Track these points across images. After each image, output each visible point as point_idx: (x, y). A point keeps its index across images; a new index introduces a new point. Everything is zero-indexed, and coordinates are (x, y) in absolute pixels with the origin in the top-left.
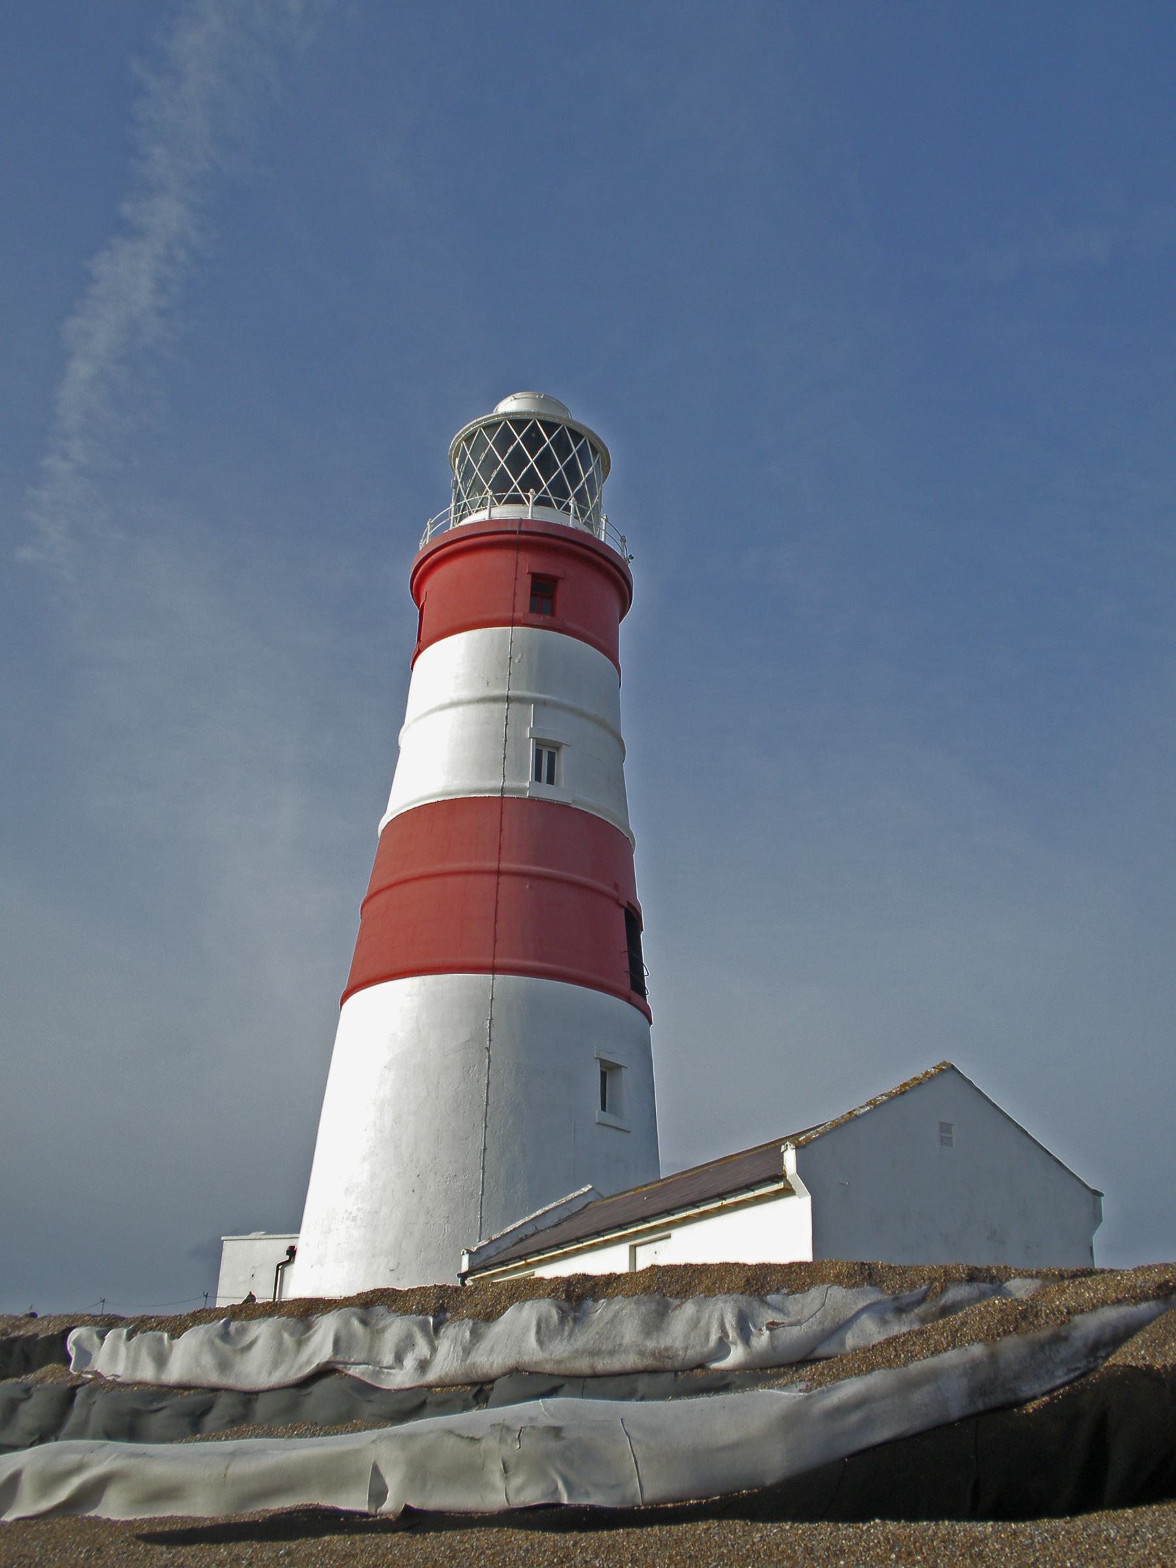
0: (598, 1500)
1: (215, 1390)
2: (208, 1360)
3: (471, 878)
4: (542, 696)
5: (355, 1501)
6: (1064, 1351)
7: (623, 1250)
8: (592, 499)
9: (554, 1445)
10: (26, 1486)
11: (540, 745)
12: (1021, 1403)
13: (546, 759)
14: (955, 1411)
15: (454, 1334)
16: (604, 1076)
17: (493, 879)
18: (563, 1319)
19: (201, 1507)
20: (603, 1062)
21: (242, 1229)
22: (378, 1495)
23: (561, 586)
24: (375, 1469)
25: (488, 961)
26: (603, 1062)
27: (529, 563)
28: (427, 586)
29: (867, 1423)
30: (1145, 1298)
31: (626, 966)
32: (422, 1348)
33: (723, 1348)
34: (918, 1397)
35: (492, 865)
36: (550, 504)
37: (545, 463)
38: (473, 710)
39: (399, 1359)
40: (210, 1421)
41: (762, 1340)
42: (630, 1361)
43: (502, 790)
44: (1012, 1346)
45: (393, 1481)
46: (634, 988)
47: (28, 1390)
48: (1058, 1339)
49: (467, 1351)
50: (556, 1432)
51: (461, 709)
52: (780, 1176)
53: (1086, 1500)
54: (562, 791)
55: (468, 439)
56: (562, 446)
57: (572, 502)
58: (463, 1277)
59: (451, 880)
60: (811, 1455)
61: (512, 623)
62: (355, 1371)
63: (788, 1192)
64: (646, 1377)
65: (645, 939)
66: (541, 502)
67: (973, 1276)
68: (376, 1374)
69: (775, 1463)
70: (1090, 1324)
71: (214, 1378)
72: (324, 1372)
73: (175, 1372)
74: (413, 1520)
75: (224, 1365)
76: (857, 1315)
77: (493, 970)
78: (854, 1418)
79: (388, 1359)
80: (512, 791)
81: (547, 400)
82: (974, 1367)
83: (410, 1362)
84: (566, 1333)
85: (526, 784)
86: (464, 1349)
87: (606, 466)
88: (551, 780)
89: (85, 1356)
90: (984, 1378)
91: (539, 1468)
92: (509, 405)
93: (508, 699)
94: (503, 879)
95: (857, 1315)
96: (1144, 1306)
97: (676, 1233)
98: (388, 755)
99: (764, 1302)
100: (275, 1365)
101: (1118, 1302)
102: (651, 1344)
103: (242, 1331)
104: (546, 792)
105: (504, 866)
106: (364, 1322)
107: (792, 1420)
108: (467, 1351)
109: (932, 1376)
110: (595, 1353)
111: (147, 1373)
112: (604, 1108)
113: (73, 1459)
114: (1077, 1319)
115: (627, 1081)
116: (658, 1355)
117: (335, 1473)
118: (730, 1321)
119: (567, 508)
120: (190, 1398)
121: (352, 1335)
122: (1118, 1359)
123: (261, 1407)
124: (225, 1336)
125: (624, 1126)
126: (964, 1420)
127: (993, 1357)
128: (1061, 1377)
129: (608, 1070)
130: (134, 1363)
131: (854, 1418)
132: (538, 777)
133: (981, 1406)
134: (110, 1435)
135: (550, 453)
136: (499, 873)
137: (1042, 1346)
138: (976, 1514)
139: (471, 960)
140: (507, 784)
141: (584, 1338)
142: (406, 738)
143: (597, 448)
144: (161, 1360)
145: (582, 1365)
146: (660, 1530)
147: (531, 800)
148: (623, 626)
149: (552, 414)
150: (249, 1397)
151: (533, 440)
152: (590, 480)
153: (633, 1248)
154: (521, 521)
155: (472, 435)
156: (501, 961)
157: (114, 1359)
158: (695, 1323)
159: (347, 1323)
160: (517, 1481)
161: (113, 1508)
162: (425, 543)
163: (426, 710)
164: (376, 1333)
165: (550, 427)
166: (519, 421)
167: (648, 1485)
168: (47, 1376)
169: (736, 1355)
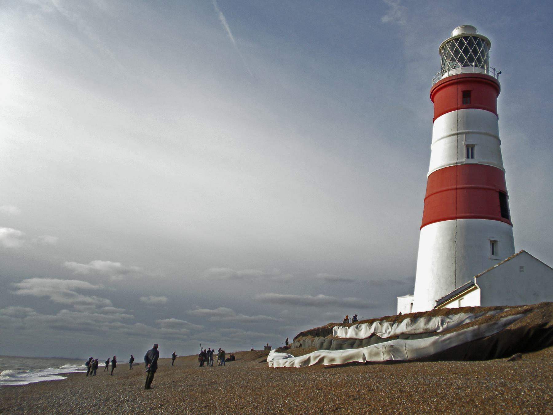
0: (399, 359)
1: (356, 339)
2: (354, 333)
3: (449, 191)
4: (467, 131)
5: (361, 360)
6: (496, 326)
7: (457, 301)
8: (483, 58)
9: (391, 349)
10: (312, 359)
11: (468, 147)
12: (485, 337)
14: (469, 340)
15: (395, 325)
17: (455, 190)
18: (411, 323)
19: (338, 362)
20: (491, 241)
21: (403, 294)
22: (364, 359)
23: (473, 93)
24: (364, 354)
25: (454, 215)
26: (491, 241)
27: (461, 88)
28: (438, 96)
29: (450, 343)
30: (520, 313)
31: (499, 209)
32: (390, 329)
33: (438, 328)
34: (461, 337)
35: (454, 187)
36: (468, 66)
37: (466, 51)
38: (447, 140)
39: (386, 331)
40: (355, 345)
41: (445, 326)
42: (421, 331)
43: (457, 163)
44: (484, 326)
45: (366, 356)
47: (325, 340)
48: (495, 324)
49: (395, 330)
50: (392, 346)
51: (444, 139)
52: (473, 285)
53: (490, 357)
55: (443, 47)
56: (470, 44)
58: (435, 307)
60: (439, 349)
61: (457, 109)
62: (378, 335)
63: (476, 288)
66: (464, 66)
67: (497, 308)
68: (382, 335)
69: (432, 351)
70: (504, 320)
71: (355, 337)
72: (373, 335)
73: (348, 336)
74: (368, 363)
75: (357, 334)
76: (466, 319)
77: (456, 218)
78: (447, 342)
79: (384, 332)
80: (460, 163)
81: (466, 27)
82: (474, 330)
83: (388, 332)
85: (463, 160)
87: (488, 44)
88: (472, 157)
89: (336, 332)
90: (476, 333)
91: (389, 352)
92: (456, 33)
93: (457, 134)
94: (458, 190)
95: (466, 319)
96: (519, 315)
97: (465, 297)
98: (428, 153)
99: (448, 317)
100: (366, 333)
101: (514, 314)
102: (425, 327)
103: (360, 326)
104: (471, 161)
105: (458, 186)
106: (380, 324)
107: (434, 343)
108: (395, 330)
109: (465, 333)
110: (415, 329)
111: (344, 336)
112: (493, 254)
113: (318, 354)
114: (502, 319)
116: (427, 329)
117: (357, 355)
118: (440, 322)
120: (352, 341)
121: (378, 327)
122: (508, 328)
123: (364, 342)
124: (357, 328)
125: (498, 258)
126: (472, 342)
127: (479, 328)
128: (495, 332)
130: (342, 334)
131: (447, 342)
132: (468, 157)
133: (476, 338)
134: (337, 349)
135: (470, 47)
136: (457, 189)
137: (491, 325)
138: (465, 360)
140: (458, 161)
141: (415, 326)
142: (433, 147)
143: (484, 40)
144: (346, 333)
145: (413, 332)
146: (279, 364)
147: (466, 165)
148: (499, 99)
149: (469, 33)
150: (361, 340)
151: (461, 44)
152: (482, 52)
153: (460, 300)
154: (457, 75)
155: (443, 46)
156: (458, 215)
157: (340, 333)
158: (434, 323)
159: (377, 324)
160: (385, 355)
161: (326, 363)
163: (440, 137)
164: (382, 326)
165: (466, 38)
166: (456, 39)
167: (408, 355)
168: (328, 338)
169: (441, 329)
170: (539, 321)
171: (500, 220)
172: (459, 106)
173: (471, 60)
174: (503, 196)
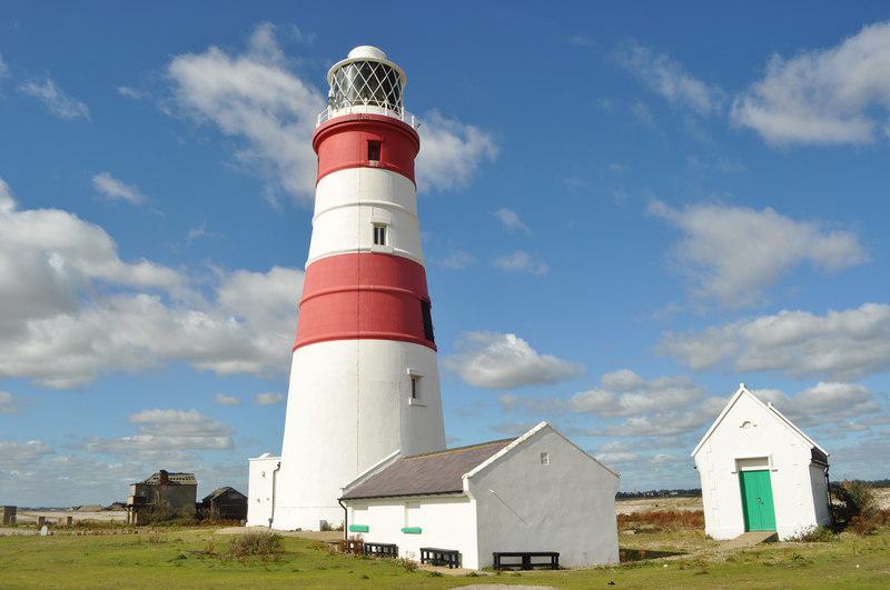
13: (379, 233)
16: (413, 381)
25: (355, 333)
37: (373, 83)
46: (427, 338)
54: (390, 246)
55: (336, 73)
57: (386, 102)
59: (336, 295)
61: (360, 166)
63: (466, 499)
64: (364, 293)
65: (432, 311)
66: (370, 103)
77: (358, 337)
84: (695, 571)
85: (367, 243)
86: (662, 523)
88: (383, 243)
104: (379, 248)
115: (423, 386)
119: (384, 106)
129: (415, 380)
132: (376, 242)
135: (376, 79)
136: (359, 290)
139: (343, 334)
151: (366, 72)
152: (396, 89)
156: (361, 333)
162: (318, 126)
165: (374, 64)
170: (410, 510)
171: (424, 344)
172: (362, 162)
173: (379, 96)
174: (426, 305)
